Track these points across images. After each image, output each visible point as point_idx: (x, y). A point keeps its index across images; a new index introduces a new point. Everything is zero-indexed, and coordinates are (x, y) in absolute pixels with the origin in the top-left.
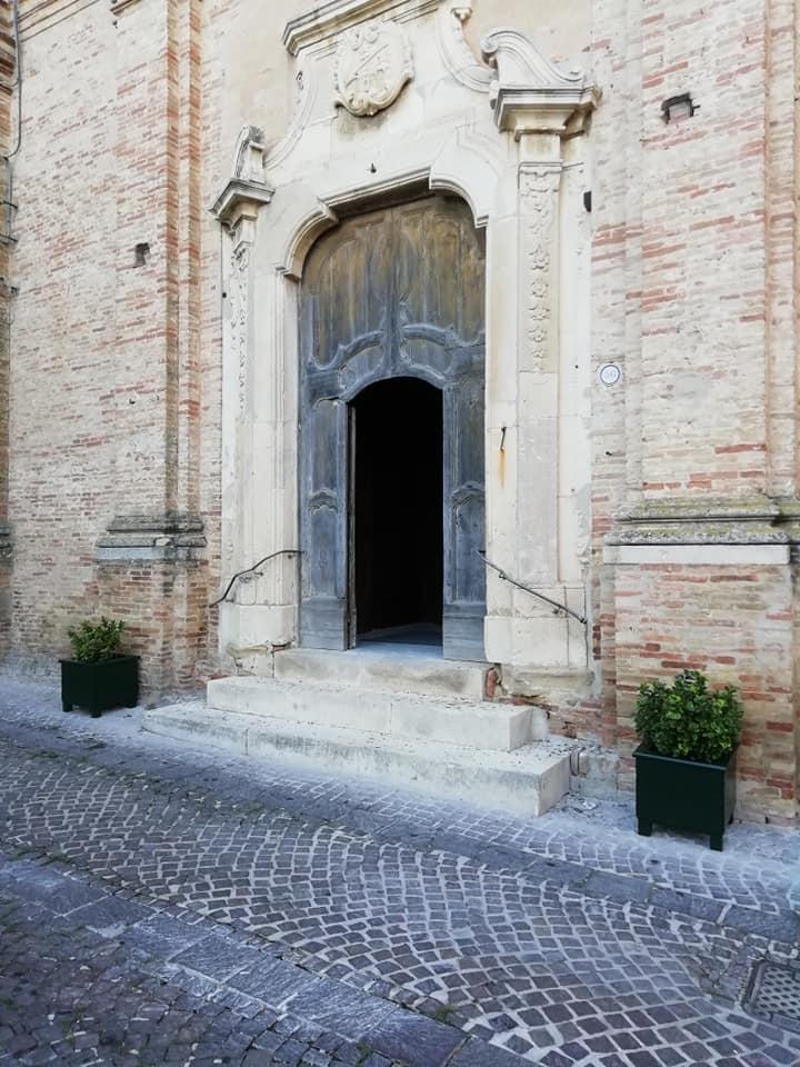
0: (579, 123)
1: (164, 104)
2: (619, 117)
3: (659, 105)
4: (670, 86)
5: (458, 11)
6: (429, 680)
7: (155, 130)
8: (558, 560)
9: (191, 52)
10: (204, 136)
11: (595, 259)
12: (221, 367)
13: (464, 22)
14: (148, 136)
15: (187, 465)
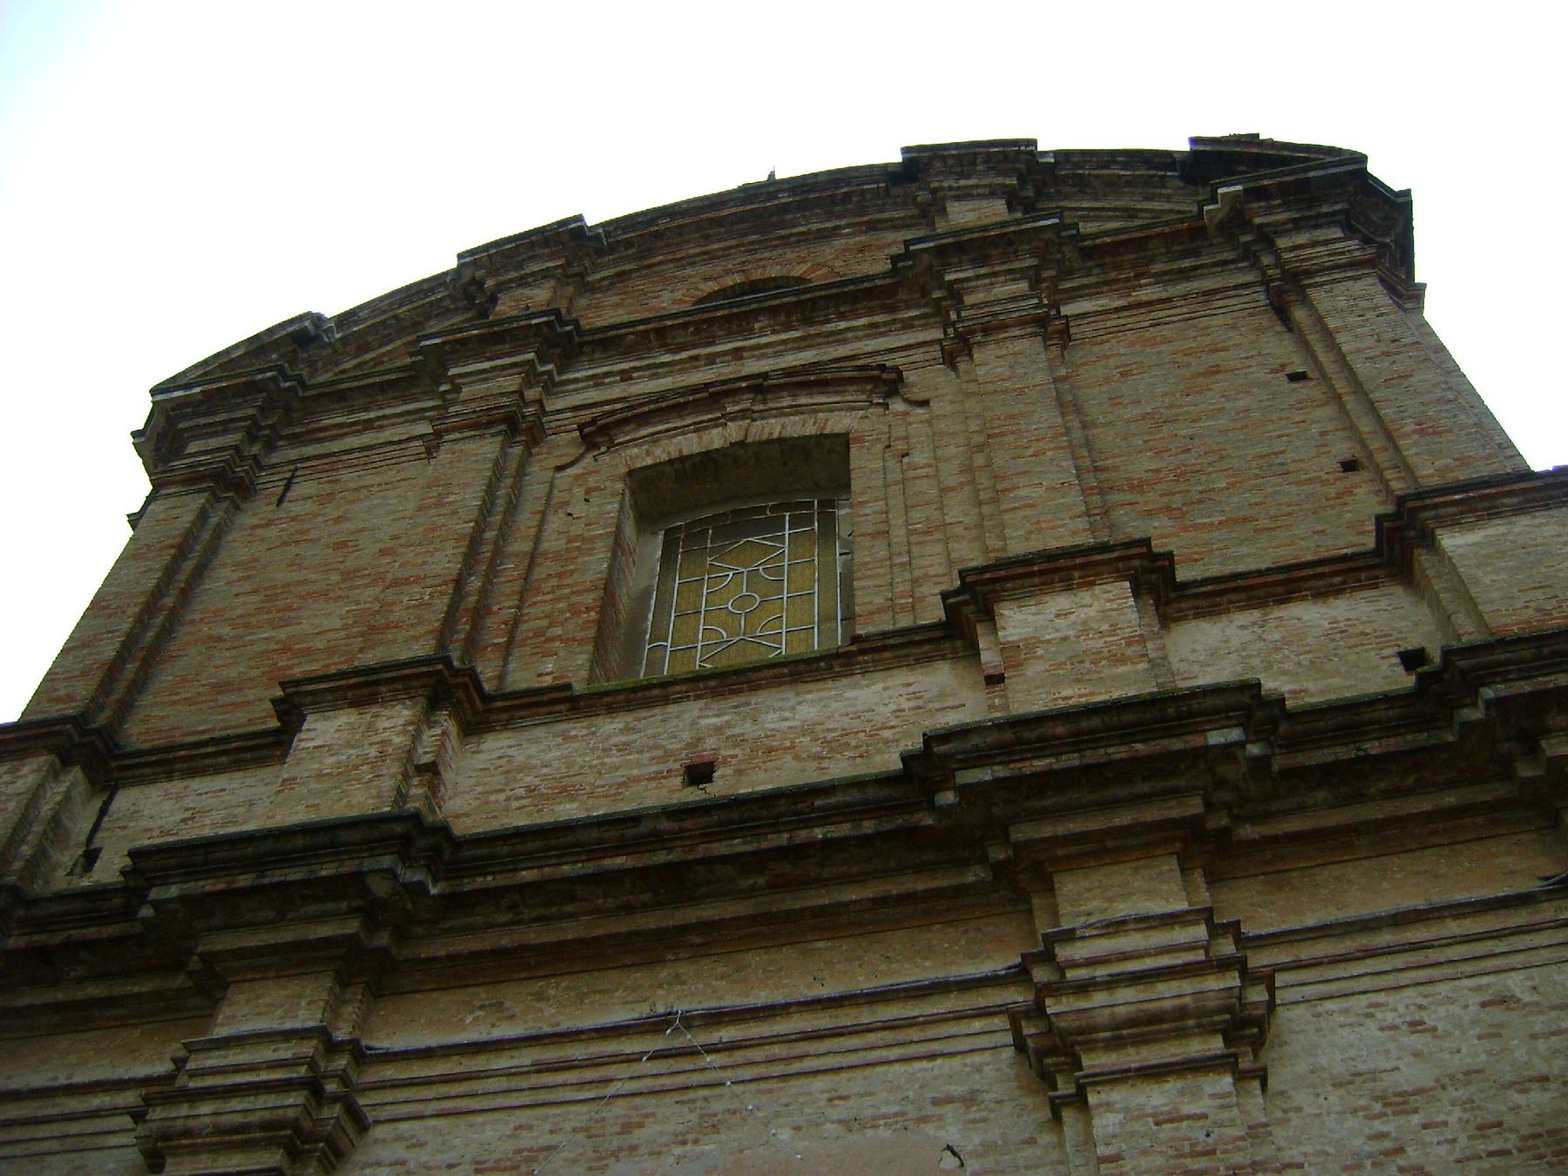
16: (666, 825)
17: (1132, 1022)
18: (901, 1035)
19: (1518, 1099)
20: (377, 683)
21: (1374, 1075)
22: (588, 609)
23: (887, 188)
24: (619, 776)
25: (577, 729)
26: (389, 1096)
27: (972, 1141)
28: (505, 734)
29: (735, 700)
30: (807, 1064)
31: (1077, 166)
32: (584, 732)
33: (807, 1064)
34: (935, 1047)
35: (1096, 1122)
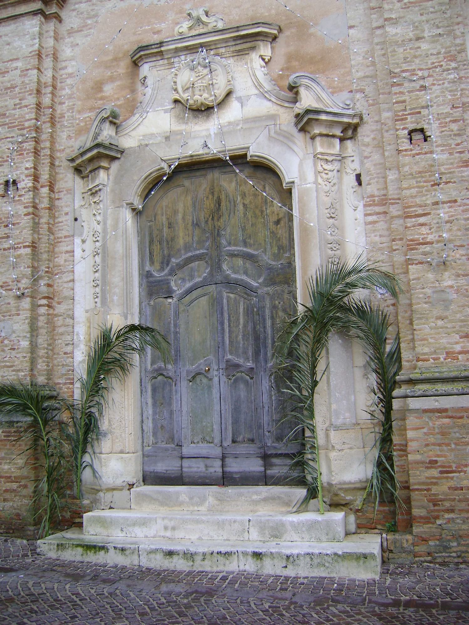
0: (350, 133)
1: (34, 86)
2: (375, 133)
3: (406, 132)
4: (412, 123)
5: (264, 57)
6: (265, 500)
7: (24, 103)
9: (54, 54)
10: (59, 109)
11: (366, 215)
13: (266, 63)
14: (18, 106)
15: (46, 346)
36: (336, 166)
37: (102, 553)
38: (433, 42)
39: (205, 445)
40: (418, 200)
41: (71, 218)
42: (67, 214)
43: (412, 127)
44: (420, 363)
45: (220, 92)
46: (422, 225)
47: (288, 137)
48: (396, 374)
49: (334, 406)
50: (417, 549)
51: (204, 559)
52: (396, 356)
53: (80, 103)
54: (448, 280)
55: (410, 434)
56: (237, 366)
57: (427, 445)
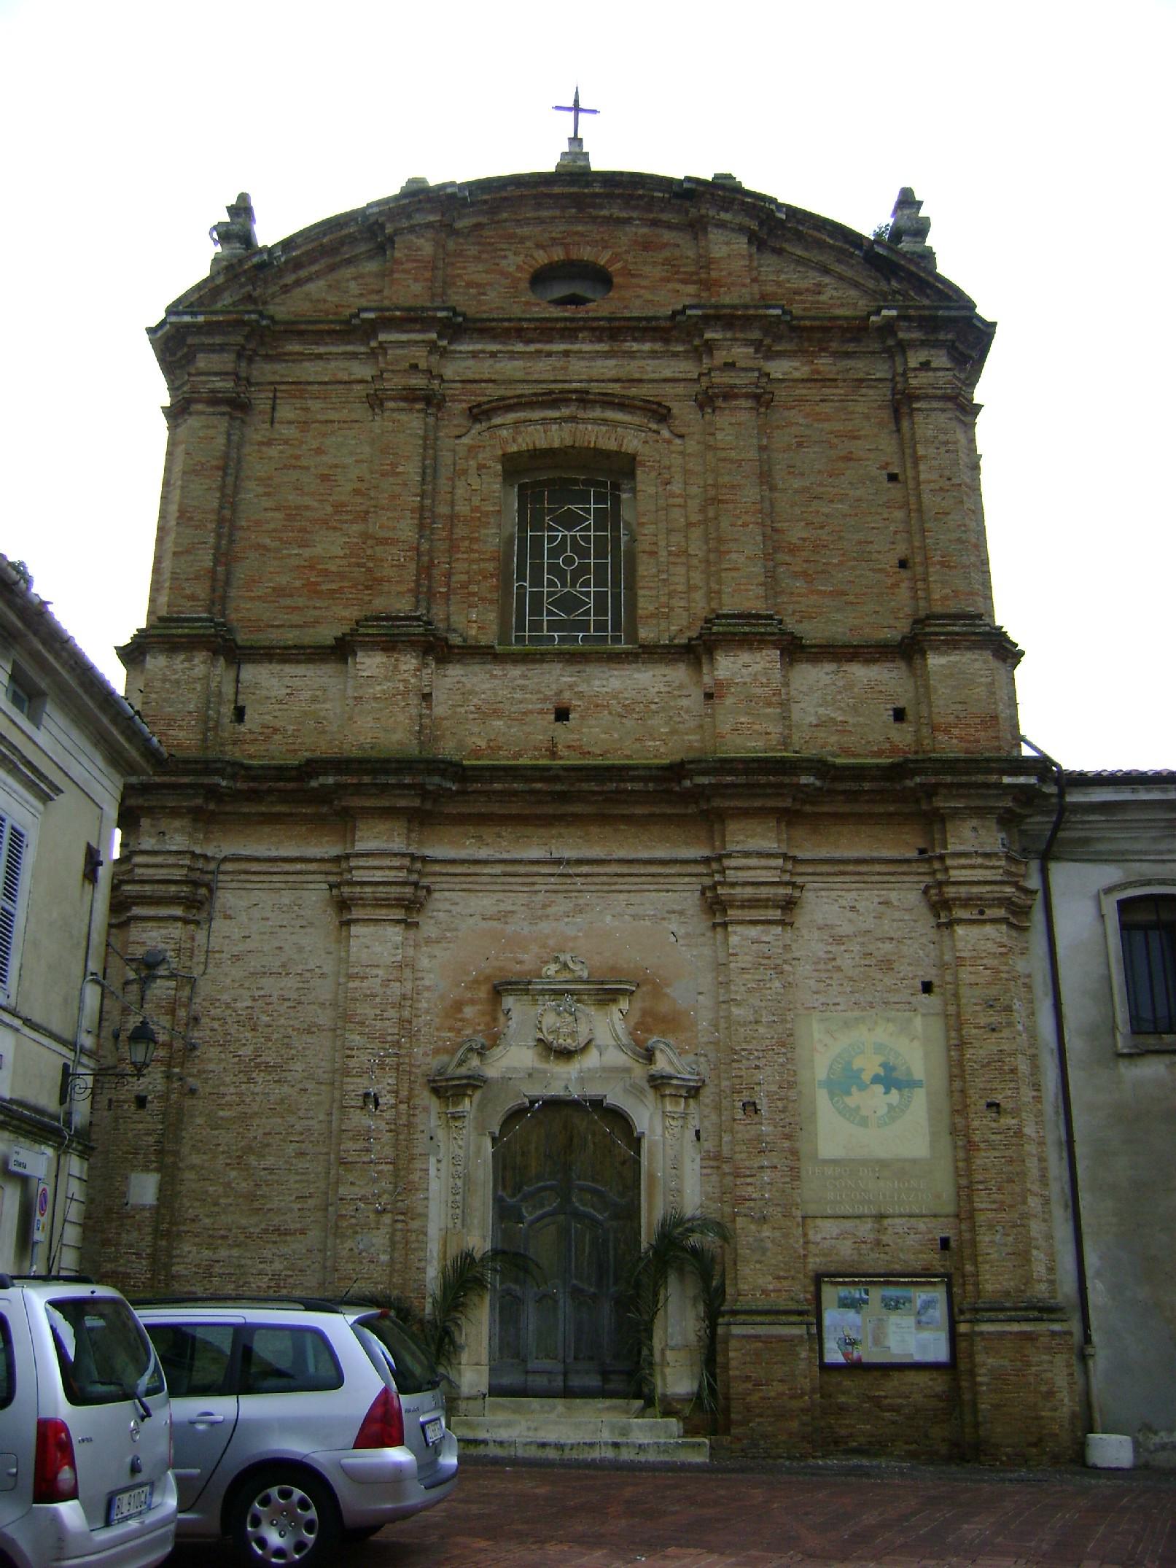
8: (100, 834)
12: (881, 1217)
16: (562, 773)
17: (749, 900)
18: (656, 880)
19: (881, 945)
20: (397, 642)
21: (832, 927)
22: (492, 576)
23: (669, 199)
24: (523, 707)
25: (497, 671)
26: (439, 879)
27: (681, 931)
28: (458, 666)
29: (579, 667)
30: (617, 887)
31: (799, 222)
32: (501, 673)
33: (617, 887)
34: (669, 887)
35: (730, 939)
36: (680, 1122)
37: (482, 1446)
38: (768, 1027)
39: (549, 1361)
40: (747, 1163)
41: (426, 1136)
42: (423, 1132)
43: (746, 1099)
44: (741, 1298)
45: (582, 1041)
46: (748, 1184)
47: (642, 1091)
48: (721, 1305)
49: (670, 1330)
50: (733, 1446)
51: (571, 1449)
52: (721, 1290)
53: (438, 1020)
54: (766, 1232)
55: (732, 1354)
56: (582, 1291)
57: (745, 1363)
